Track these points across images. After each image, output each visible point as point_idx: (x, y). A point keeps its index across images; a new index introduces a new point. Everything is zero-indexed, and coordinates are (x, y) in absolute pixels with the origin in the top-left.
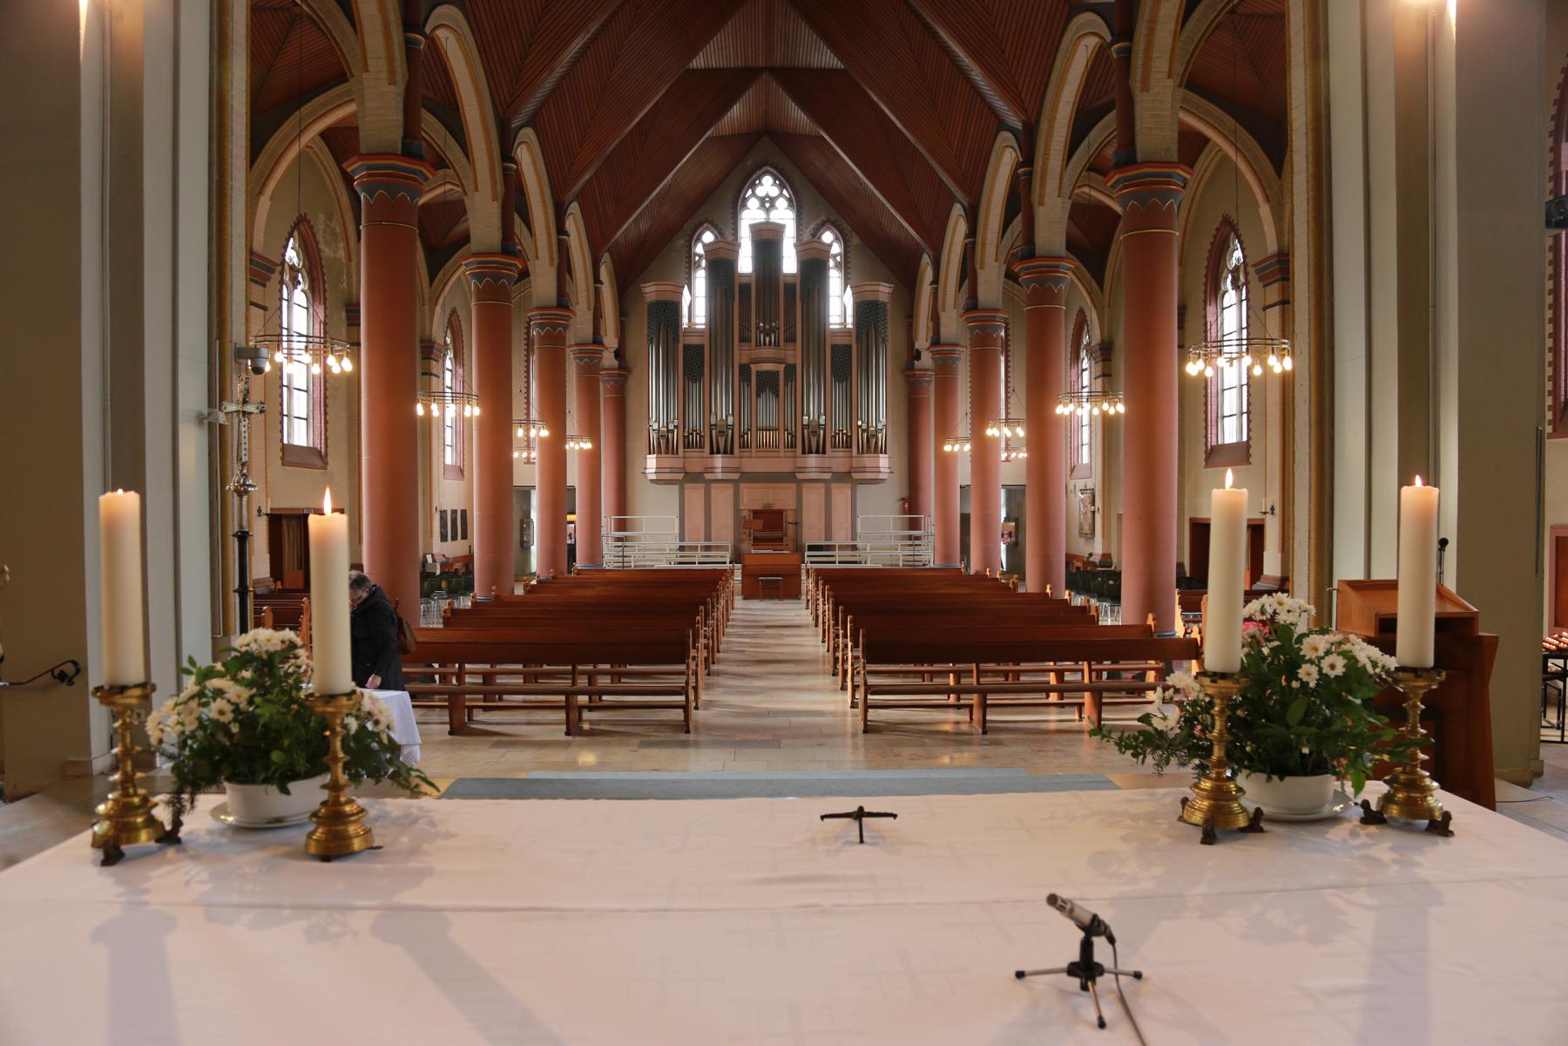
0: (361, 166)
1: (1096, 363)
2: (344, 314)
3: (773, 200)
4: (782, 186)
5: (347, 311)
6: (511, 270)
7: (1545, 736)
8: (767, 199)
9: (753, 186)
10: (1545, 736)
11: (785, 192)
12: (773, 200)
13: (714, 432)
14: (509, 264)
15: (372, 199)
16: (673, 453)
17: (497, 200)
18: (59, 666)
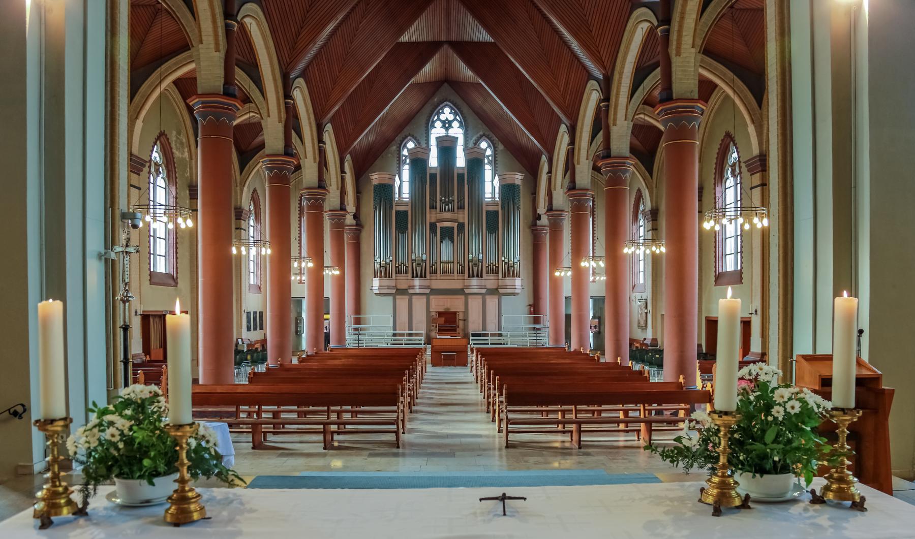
2: (188, 192)
3: (450, 122)
5: (190, 190)
8: (447, 122)
13: (414, 264)
16: (389, 277)
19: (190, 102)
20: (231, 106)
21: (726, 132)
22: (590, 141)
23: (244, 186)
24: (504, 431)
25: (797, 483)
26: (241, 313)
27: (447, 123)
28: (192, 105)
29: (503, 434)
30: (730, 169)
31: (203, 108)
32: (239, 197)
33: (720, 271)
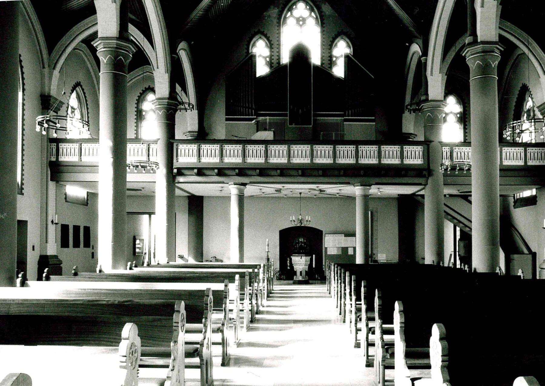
0: (100, 43)
1: (543, 194)
3: (304, 20)
4: (312, 10)
6: (127, 48)
7: (268, 313)
8: (301, 19)
9: (290, 9)
10: (268, 313)
11: (313, 14)
12: (304, 20)
14: (126, 47)
15: (105, 60)
17: (115, 2)
18: (47, 221)
19: (94, 44)
20: (126, 48)
21: (523, 84)
22: (442, 60)
23: (54, 68)
24: (363, 344)
25: (207, 138)
26: (47, 225)
27: (301, 21)
28: (96, 46)
29: (363, 349)
30: (526, 115)
31: (104, 48)
32: (46, 82)
33: (518, 197)
